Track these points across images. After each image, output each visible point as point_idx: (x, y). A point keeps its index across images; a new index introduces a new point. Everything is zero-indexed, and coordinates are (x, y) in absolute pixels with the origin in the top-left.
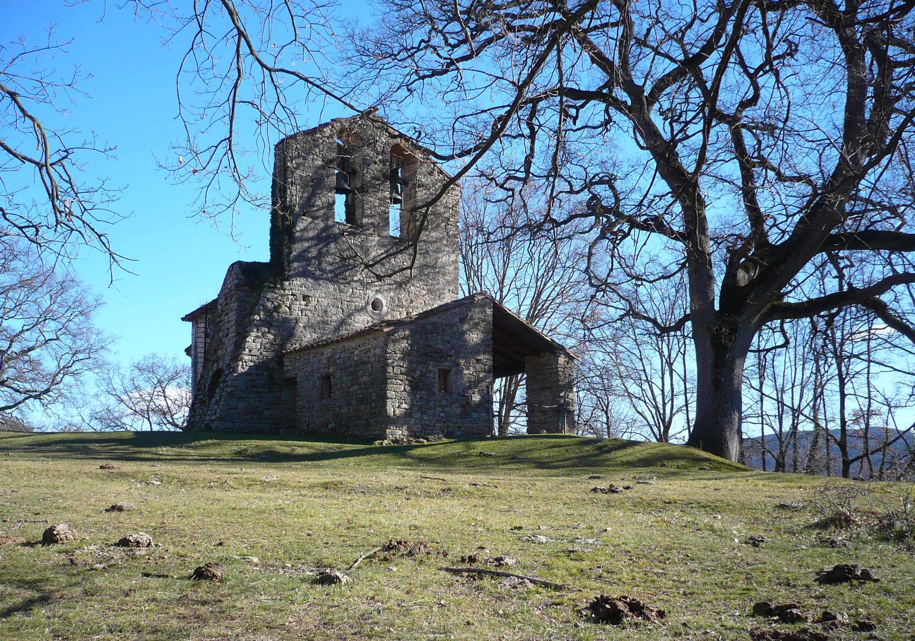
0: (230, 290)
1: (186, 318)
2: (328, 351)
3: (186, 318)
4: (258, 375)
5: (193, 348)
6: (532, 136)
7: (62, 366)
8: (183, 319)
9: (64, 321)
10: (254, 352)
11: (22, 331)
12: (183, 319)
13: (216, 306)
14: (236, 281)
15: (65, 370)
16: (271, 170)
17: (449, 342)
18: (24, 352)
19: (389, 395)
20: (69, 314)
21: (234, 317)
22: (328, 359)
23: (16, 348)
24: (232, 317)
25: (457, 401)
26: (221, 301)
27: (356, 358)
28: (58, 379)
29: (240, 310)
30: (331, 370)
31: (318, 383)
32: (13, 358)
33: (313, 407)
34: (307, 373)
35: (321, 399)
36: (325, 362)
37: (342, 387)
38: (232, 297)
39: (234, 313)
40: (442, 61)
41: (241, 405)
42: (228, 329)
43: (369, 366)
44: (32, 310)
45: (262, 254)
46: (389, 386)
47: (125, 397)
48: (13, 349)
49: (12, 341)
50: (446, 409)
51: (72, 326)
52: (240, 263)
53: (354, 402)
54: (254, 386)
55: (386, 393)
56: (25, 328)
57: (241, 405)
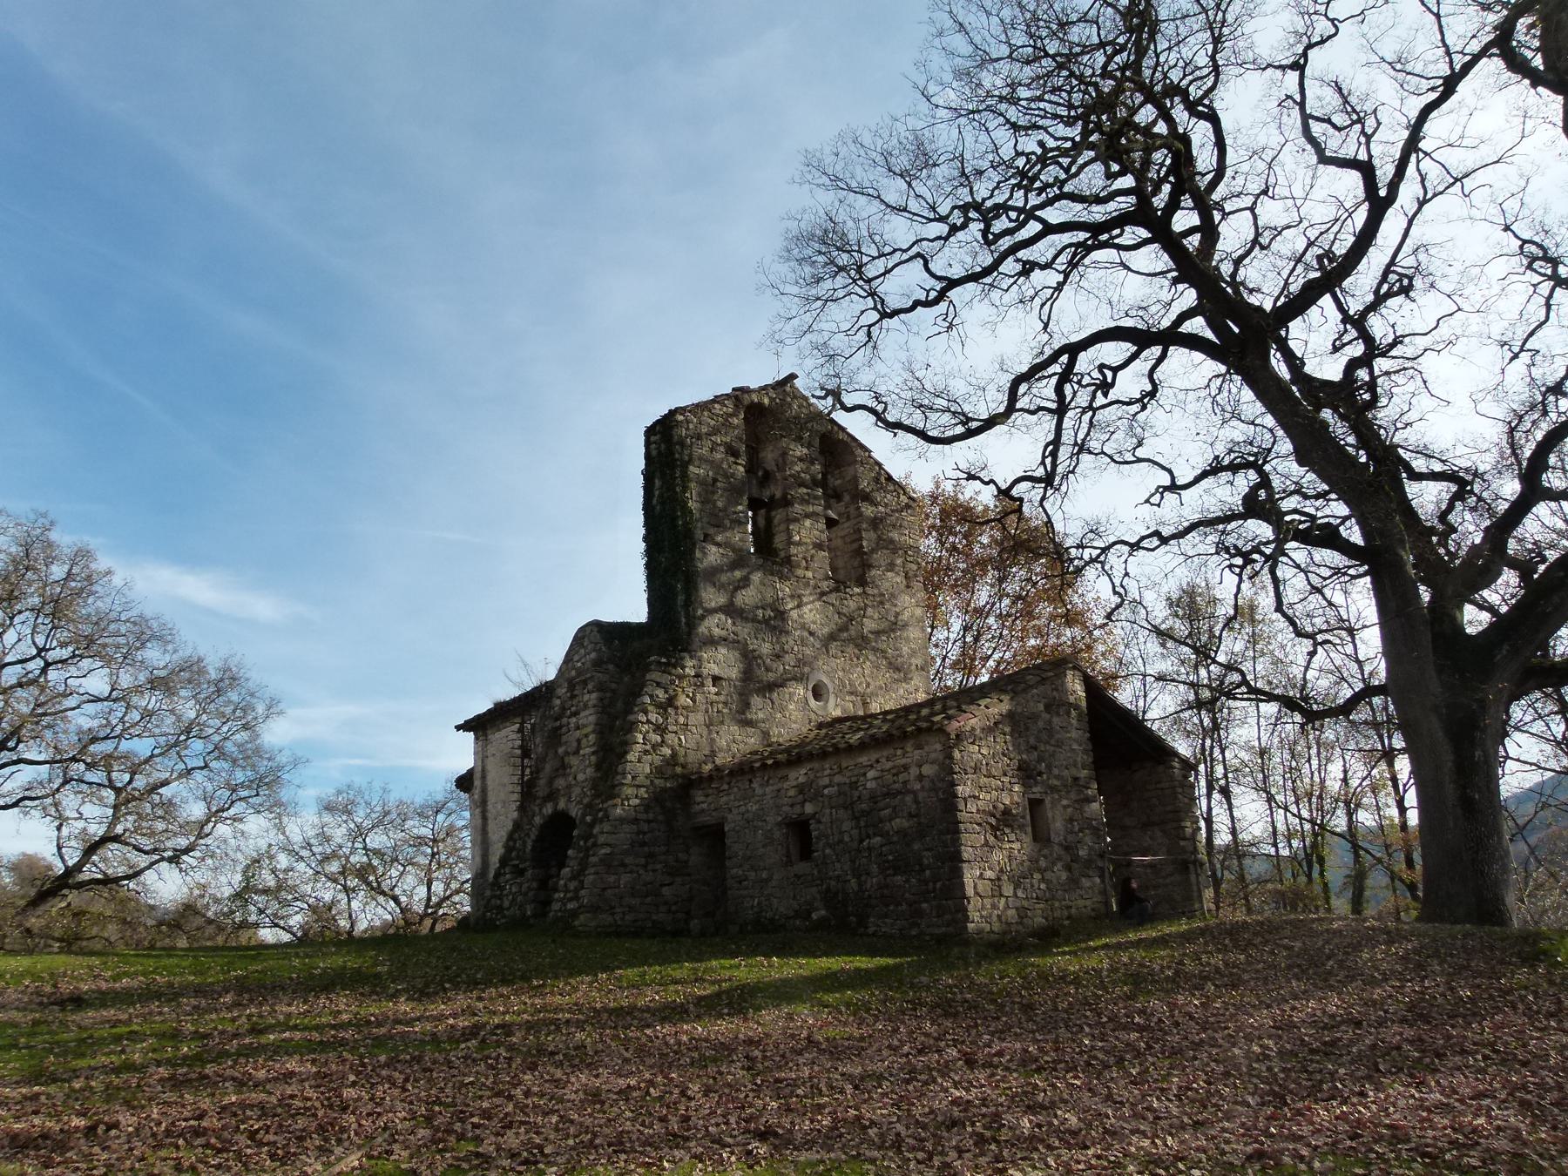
0: (580, 672)
1: (465, 727)
2: (799, 775)
3: (465, 727)
4: (649, 822)
5: (477, 775)
6: (1061, 410)
7: (214, 809)
8: (458, 728)
9: (216, 738)
10: (641, 780)
11: (152, 756)
12: (458, 728)
13: (549, 700)
14: (593, 655)
15: (215, 815)
16: (1365, 260)
17: (1035, 748)
18: (154, 788)
19: (965, 856)
20: (225, 729)
21: (592, 719)
22: (801, 789)
23: (140, 782)
24: (588, 718)
25: (1059, 859)
26: (562, 691)
27: (869, 785)
28: (207, 829)
29: (604, 708)
30: (809, 808)
31: (777, 834)
32: (134, 799)
33: (770, 879)
34: (750, 816)
35: (789, 863)
36: (792, 793)
37: (841, 841)
38: (585, 683)
39: (591, 711)
40: (932, 282)
41: (625, 879)
42: (579, 741)
43: (909, 798)
44: (168, 724)
45: (632, 606)
46: (964, 836)
47: (305, 853)
48: (134, 784)
49: (133, 773)
50: (1048, 875)
51: (229, 746)
52: (596, 625)
53: (874, 868)
54: (643, 844)
55: (959, 853)
56: (157, 751)
57: (625, 879)
